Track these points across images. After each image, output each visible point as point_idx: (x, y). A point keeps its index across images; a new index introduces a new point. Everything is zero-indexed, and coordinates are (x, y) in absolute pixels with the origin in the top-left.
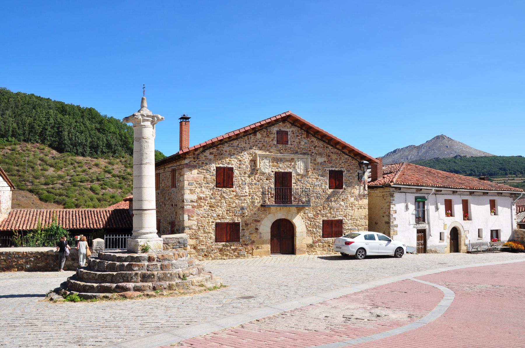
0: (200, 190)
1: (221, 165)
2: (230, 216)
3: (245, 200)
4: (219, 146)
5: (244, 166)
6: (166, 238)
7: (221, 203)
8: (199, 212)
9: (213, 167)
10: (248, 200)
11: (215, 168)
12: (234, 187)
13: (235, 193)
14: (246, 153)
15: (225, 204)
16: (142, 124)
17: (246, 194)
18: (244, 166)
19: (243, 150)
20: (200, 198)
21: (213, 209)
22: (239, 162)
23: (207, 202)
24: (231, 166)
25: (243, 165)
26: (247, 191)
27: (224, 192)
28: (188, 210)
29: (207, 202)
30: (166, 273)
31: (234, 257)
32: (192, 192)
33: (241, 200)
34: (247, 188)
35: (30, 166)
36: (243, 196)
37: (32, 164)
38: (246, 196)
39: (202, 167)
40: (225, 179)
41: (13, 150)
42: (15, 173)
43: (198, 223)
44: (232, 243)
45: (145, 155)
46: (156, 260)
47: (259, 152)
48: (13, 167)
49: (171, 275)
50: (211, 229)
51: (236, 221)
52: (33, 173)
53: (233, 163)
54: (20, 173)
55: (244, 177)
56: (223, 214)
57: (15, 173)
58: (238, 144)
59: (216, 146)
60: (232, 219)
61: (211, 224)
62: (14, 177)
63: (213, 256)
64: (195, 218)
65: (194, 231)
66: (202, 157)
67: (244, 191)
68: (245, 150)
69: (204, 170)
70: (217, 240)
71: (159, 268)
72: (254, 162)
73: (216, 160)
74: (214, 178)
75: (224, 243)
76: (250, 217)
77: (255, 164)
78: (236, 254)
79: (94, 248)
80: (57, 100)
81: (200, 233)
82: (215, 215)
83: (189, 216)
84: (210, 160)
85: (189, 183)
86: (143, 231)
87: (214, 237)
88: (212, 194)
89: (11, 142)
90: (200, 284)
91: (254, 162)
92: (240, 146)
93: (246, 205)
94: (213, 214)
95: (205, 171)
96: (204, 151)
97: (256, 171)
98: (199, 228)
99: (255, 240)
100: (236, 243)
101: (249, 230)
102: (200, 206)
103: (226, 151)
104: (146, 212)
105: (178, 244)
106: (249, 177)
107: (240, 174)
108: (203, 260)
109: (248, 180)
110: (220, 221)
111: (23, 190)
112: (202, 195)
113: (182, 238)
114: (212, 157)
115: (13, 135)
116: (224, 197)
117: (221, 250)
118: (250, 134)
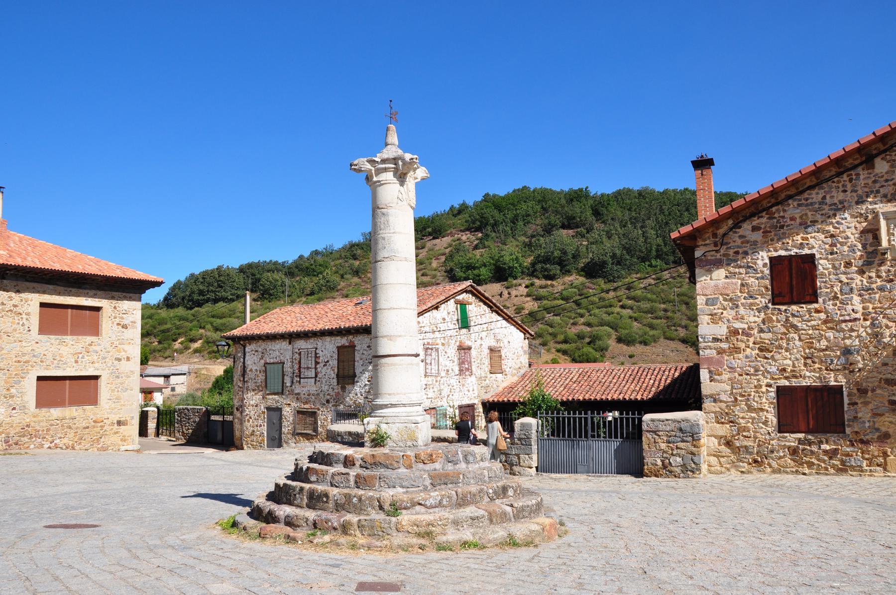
0: (733, 313)
1: (783, 253)
2: (814, 371)
3: (852, 330)
4: (774, 209)
5: (846, 248)
6: (653, 420)
7: (788, 340)
8: (735, 363)
9: (763, 258)
10: (863, 329)
11: (767, 261)
12: (820, 300)
13: (823, 316)
14: (846, 215)
15: (798, 343)
16: (375, 179)
17: (854, 316)
18: (846, 248)
19: (839, 208)
20: (735, 332)
21: (769, 355)
22: (829, 240)
23: (752, 340)
24: (809, 252)
25: (842, 244)
26: (859, 307)
27: (793, 315)
28: (709, 360)
29: (752, 340)
30: (350, 495)
31: (832, 471)
32: (715, 318)
33: (843, 330)
34: (856, 299)
35: (683, 301)
36: (845, 321)
37: (685, 298)
38: (855, 320)
39: (736, 261)
40: (794, 282)
41: (659, 279)
42: (661, 313)
43: (732, 388)
44: (822, 437)
45: (381, 242)
46: (358, 464)
47: (883, 208)
48: (657, 305)
49: (360, 500)
50: (767, 401)
51: (833, 383)
52: (688, 313)
53: (814, 243)
54: (669, 314)
55: (845, 273)
56: (794, 366)
57: (661, 313)
58: (824, 198)
59: (767, 209)
60: (819, 378)
61: (764, 389)
62: (659, 321)
63: (774, 464)
64: (726, 376)
65: (723, 405)
66: (735, 239)
67: (849, 307)
68: (843, 209)
69: (740, 267)
70: (783, 427)
71: (352, 483)
72: (871, 233)
73: (767, 242)
74: (767, 282)
75: (801, 436)
76: (870, 371)
77: (877, 238)
78: (838, 463)
79: (516, 435)
80: (724, 191)
81: (739, 411)
82: (774, 369)
83: (710, 372)
84: (755, 243)
85: (707, 300)
86: (379, 401)
87: (775, 420)
88: (764, 322)
89: (656, 266)
90: (422, 530)
91: (871, 233)
92: (828, 200)
93: (857, 342)
94: (768, 368)
95: (743, 271)
96: (737, 226)
97: (879, 257)
98: (736, 399)
99: (891, 431)
100: (833, 437)
101: (871, 406)
102: (737, 350)
103: (793, 219)
104: (384, 360)
105: (678, 434)
106: (861, 272)
107: (834, 267)
108: (749, 472)
109: (858, 281)
110: (787, 384)
111: (672, 339)
112: (738, 325)
113: (687, 421)
114: (757, 236)
115: (658, 257)
116: (794, 327)
117: (794, 452)
118: (855, 167)
